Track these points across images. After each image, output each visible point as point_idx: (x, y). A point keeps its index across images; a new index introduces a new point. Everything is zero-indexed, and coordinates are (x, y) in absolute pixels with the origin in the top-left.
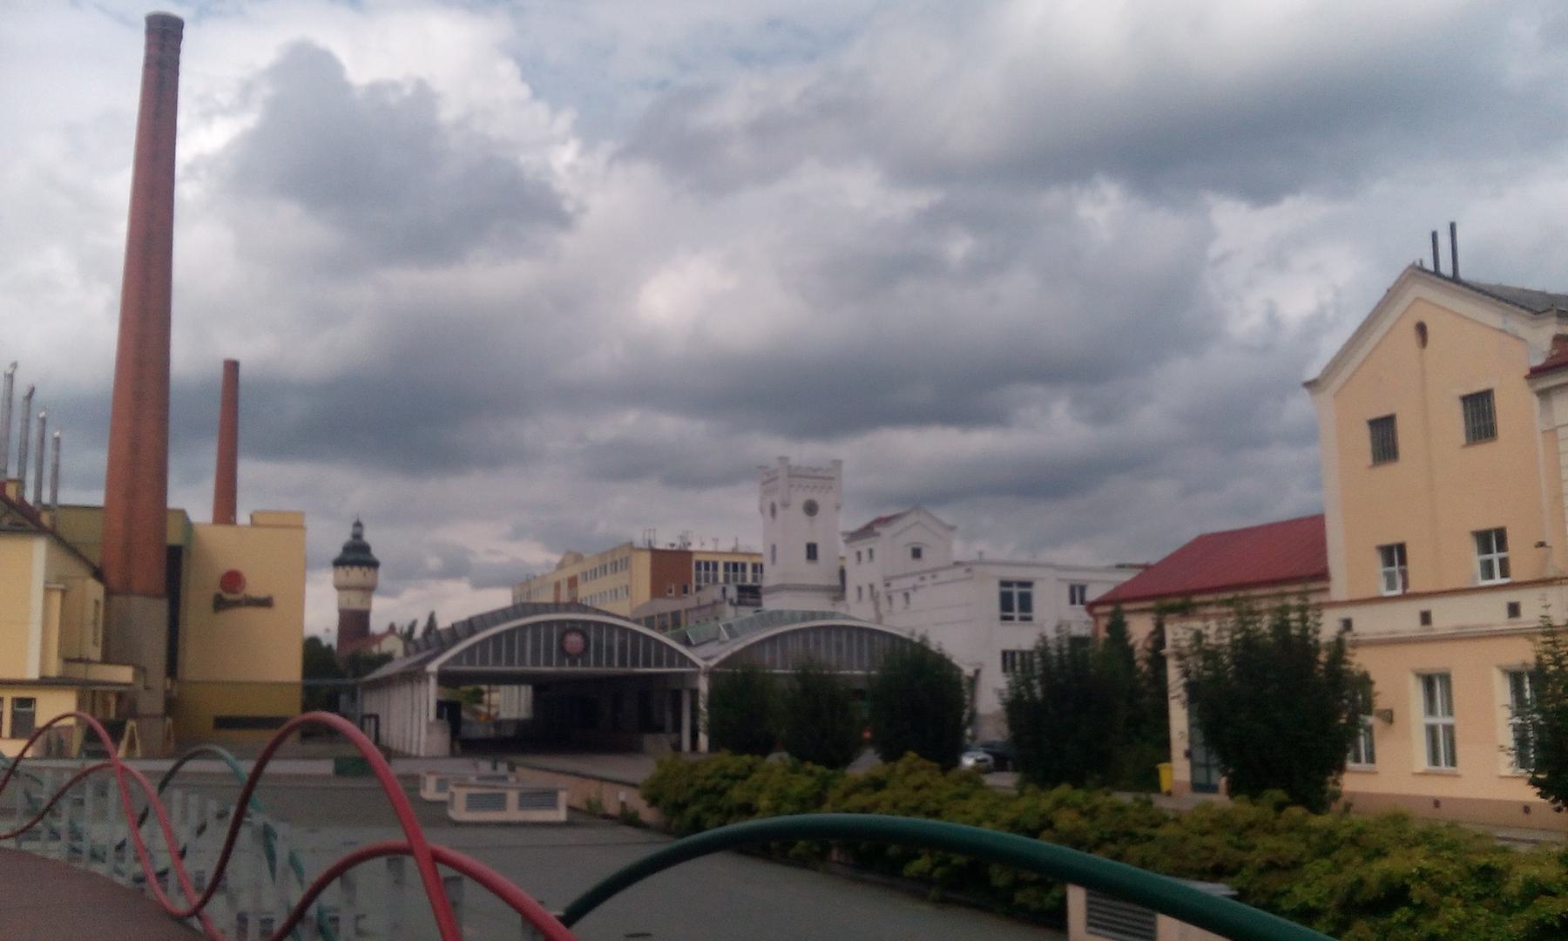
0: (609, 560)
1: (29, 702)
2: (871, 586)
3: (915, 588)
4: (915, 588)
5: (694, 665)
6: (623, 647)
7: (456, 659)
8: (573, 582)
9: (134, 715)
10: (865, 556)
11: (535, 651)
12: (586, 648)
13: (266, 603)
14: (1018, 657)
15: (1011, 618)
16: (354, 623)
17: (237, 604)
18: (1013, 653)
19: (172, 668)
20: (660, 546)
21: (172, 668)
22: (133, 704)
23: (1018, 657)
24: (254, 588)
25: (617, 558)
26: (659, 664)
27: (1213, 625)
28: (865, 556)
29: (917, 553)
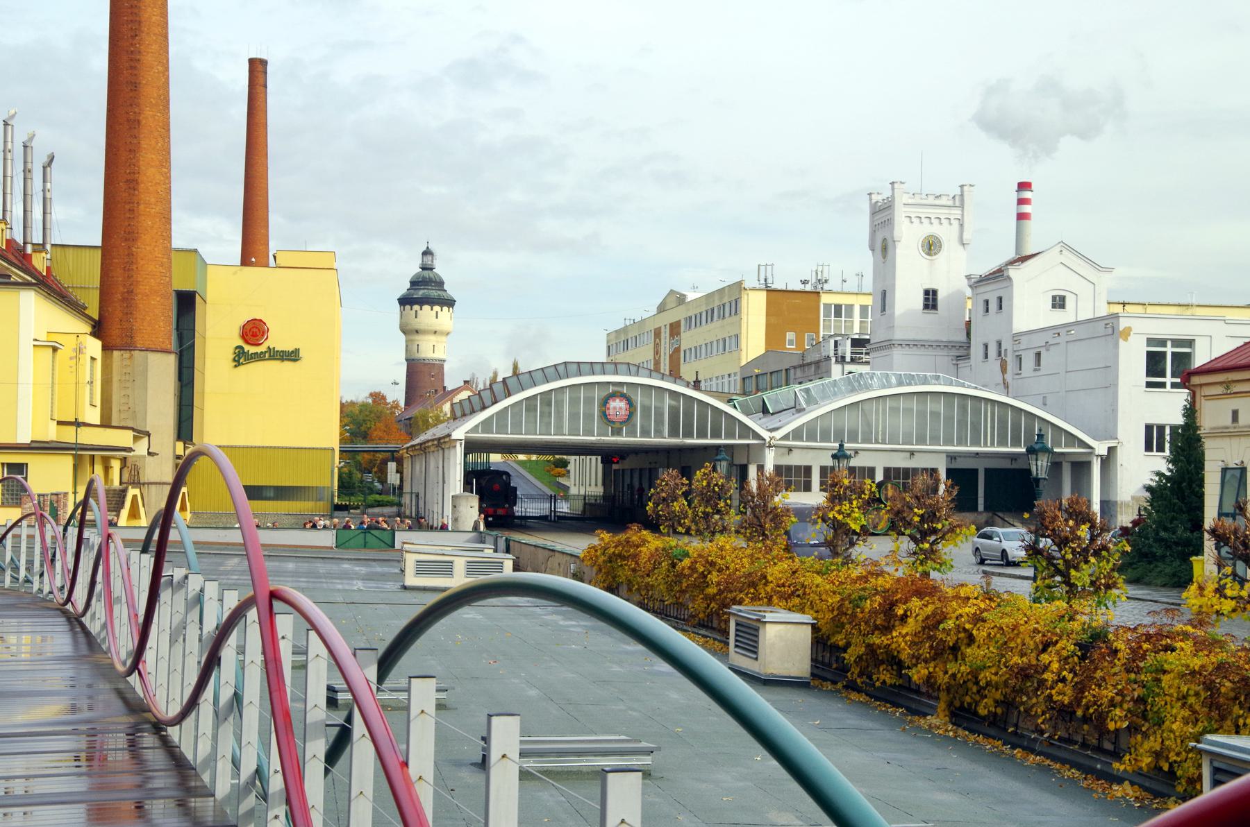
0: (717, 303)
1: (20, 468)
2: (999, 344)
3: (1047, 345)
4: (1047, 345)
5: (757, 436)
6: (674, 413)
7: (486, 425)
8: (675, 329)
9: (137, 483)
10: (993, 306)
11: (574, 416)
12: (631, 415)
13: (292, 356)
14: (1168, 431)
15: (1163, 385)
16: (421, 376)
17: (259, 357)
18: (1161, 428)
19: (184, 429)
20: (778, 285)
21: (184, 429)
22: (136, 470)
23: (1168, 431)
24: (277, 339)
25: (726, 300)
26: (716, 434)
27: (26, 639)
28: (993, 306)
29: (1059, 302)
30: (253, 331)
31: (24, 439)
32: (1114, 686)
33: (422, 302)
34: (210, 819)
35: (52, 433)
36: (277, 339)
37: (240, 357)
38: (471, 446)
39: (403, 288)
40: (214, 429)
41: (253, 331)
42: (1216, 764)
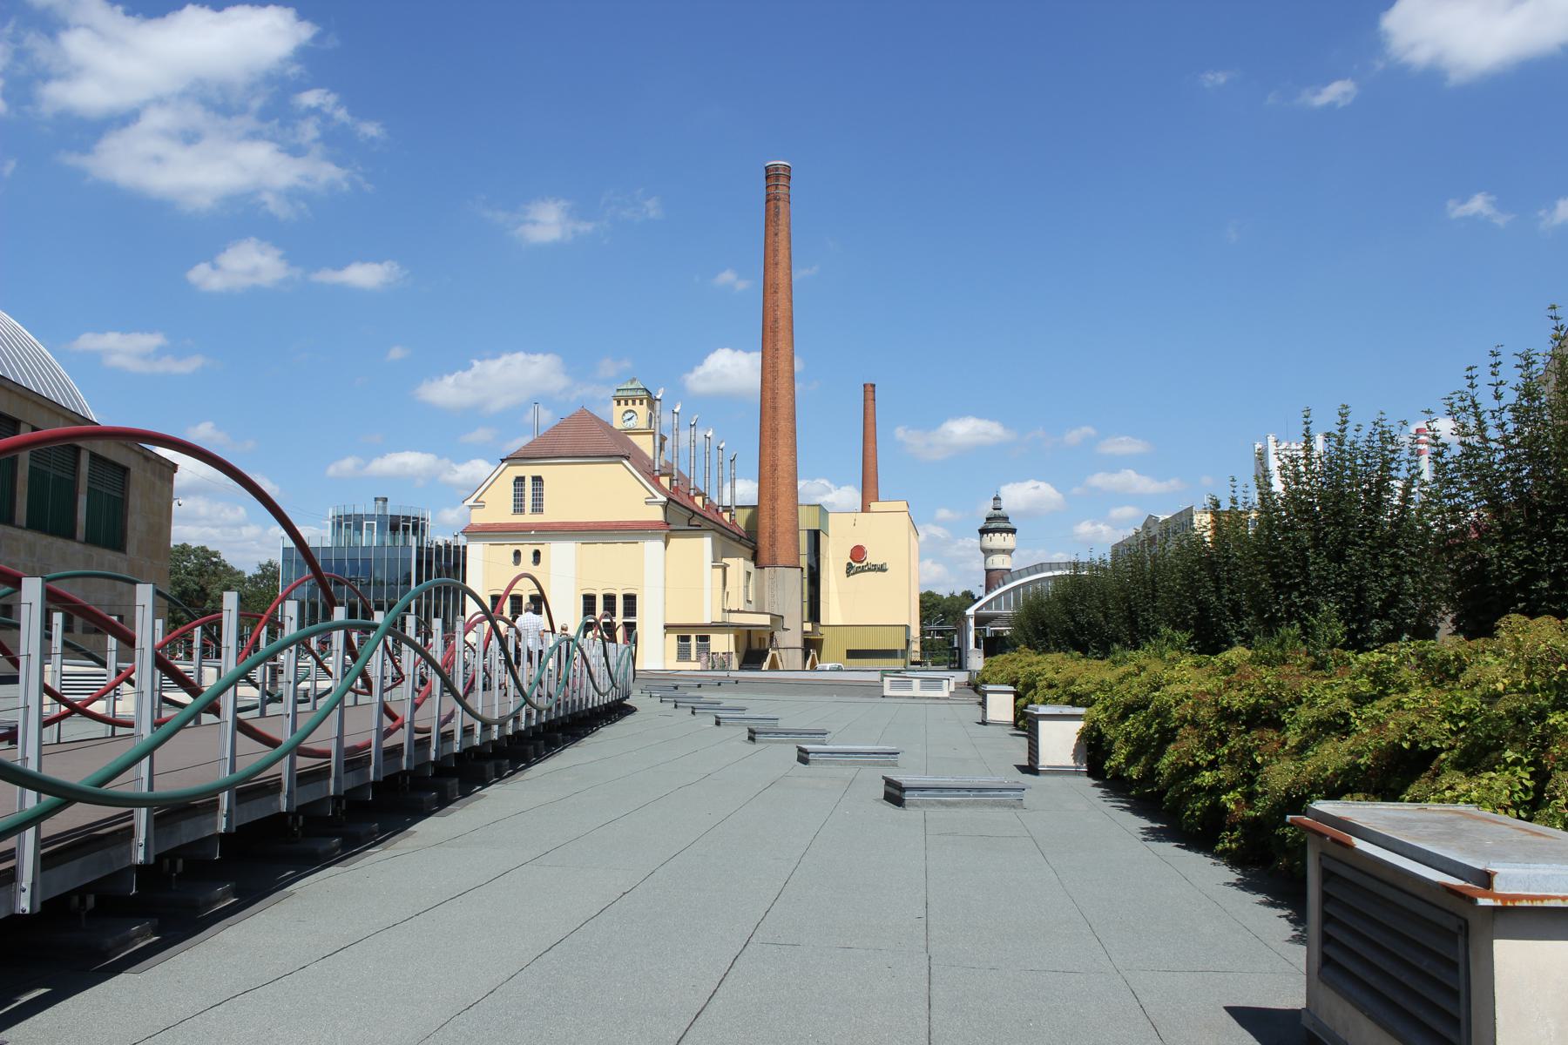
13: (882, 569)
17: (863, 570)
30: (858, 553)
31: (708, 621)
32: (1279, 675)
33: (994, 531)
34: (1208, 536)
35: (718, 618)
36: (872, 558)
37: (850, 570)
38: (981, 621)
39: (981, 524)
40: (833, 611)
41: (858, 553)
42: (1332, 930)
